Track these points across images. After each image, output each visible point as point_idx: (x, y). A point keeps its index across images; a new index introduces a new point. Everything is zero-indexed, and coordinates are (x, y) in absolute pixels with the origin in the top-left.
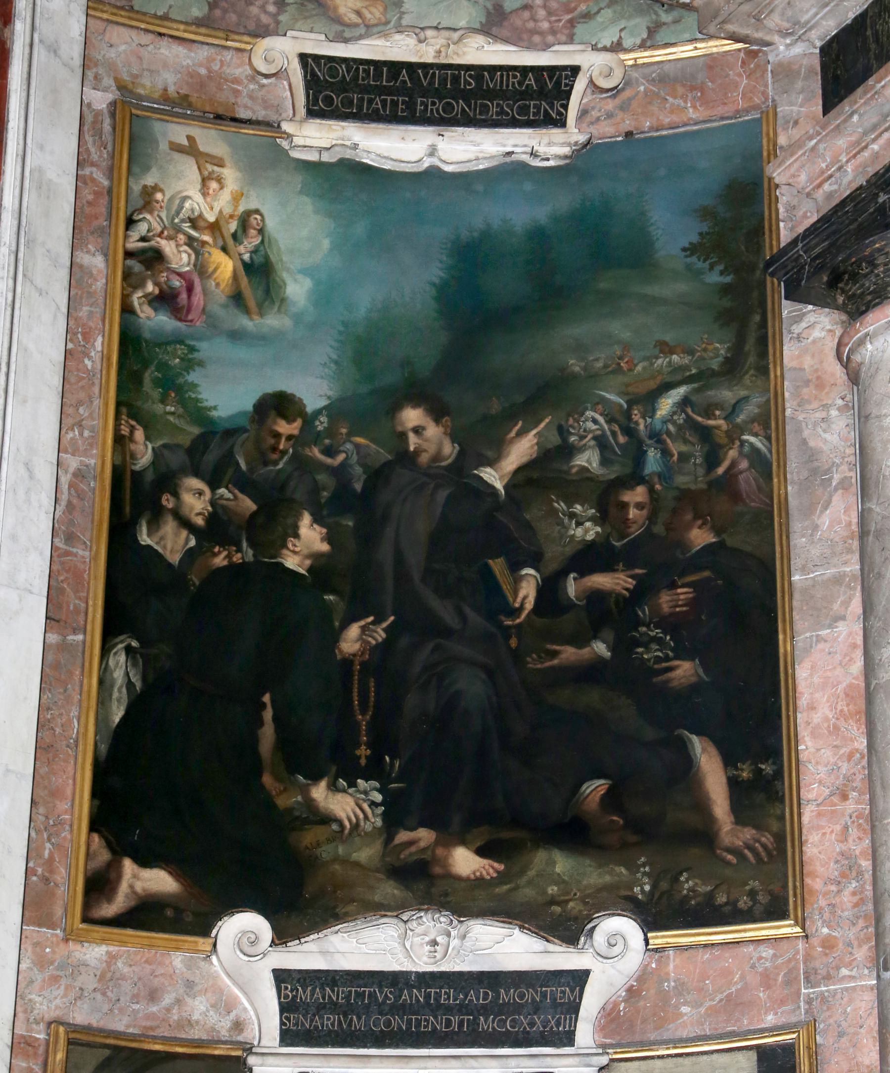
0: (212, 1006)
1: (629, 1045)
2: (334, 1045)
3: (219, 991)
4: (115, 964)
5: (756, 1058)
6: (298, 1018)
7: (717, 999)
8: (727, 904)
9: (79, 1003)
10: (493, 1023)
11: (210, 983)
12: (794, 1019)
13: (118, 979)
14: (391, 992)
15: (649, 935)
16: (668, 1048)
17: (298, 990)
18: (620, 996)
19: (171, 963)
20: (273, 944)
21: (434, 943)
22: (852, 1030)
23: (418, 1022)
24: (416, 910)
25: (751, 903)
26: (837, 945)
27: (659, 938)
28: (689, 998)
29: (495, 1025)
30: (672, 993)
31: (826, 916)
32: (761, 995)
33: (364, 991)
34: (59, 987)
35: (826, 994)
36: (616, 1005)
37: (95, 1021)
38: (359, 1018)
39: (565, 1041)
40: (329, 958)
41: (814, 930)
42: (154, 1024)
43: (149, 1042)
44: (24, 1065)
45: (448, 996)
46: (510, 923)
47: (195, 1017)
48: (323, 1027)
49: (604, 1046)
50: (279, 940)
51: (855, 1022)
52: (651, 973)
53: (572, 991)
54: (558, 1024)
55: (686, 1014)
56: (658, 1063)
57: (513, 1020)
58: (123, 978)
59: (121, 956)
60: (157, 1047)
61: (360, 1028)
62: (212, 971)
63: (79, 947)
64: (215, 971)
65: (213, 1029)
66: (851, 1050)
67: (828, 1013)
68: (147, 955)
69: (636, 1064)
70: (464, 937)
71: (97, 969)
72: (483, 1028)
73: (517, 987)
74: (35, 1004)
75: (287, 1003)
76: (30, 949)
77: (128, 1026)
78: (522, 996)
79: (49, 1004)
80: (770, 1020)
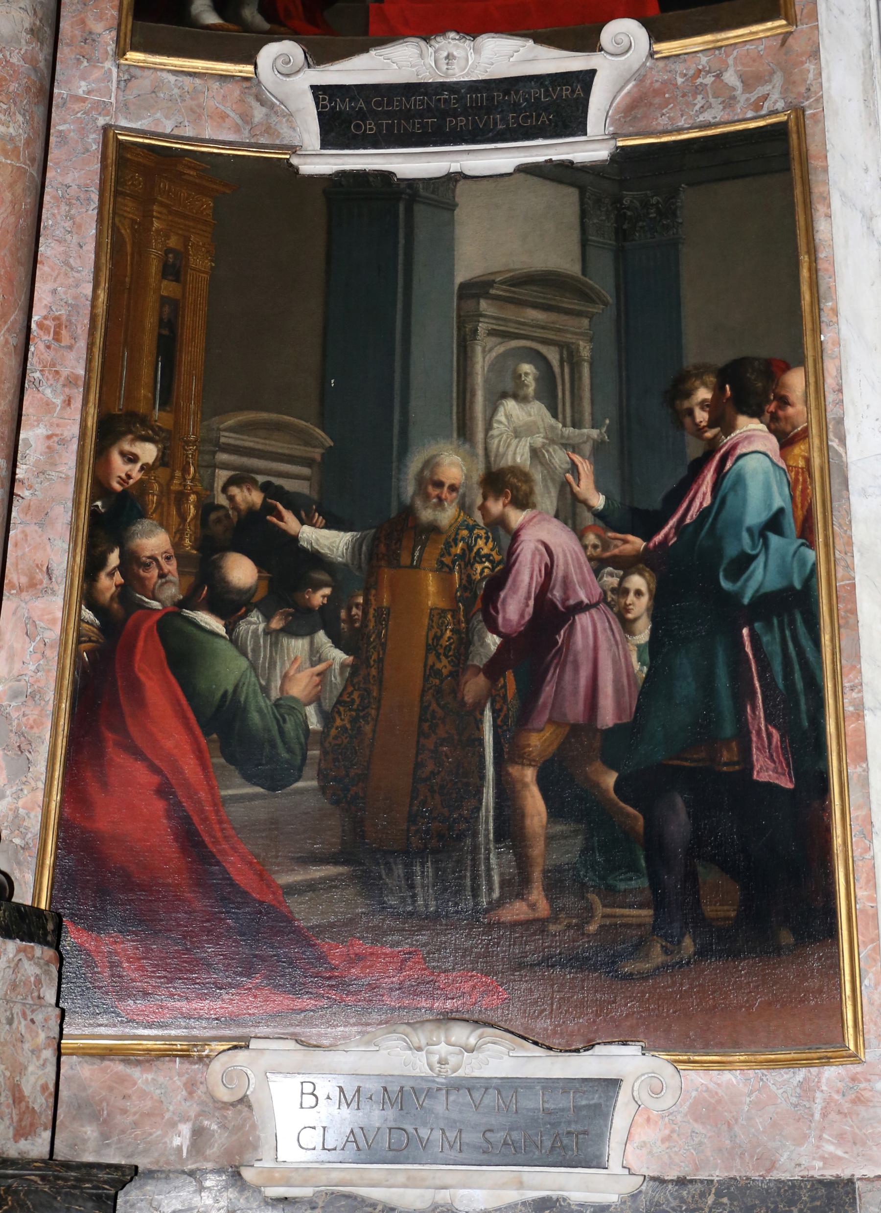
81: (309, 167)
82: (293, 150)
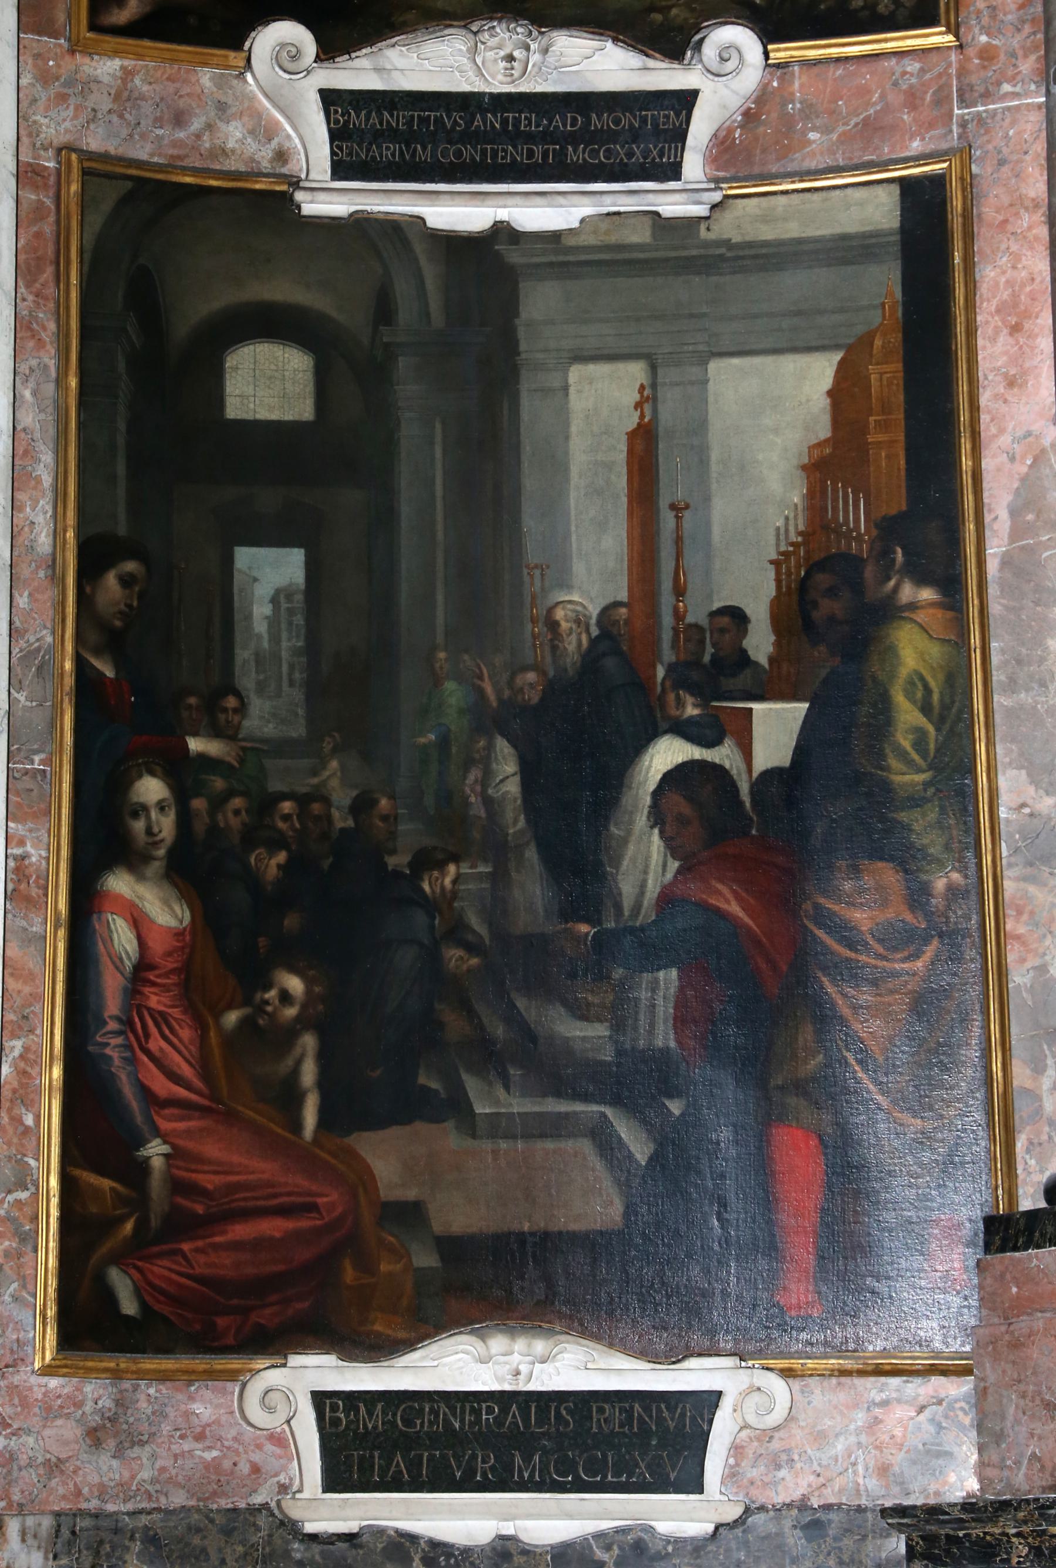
0: (249, 133)
1: (746, 179)
2: (395, 180)
3: (257, 115)
4: (132, 80)
5: (898, 192)
6: (352, 147)
7: (852, 123)
8: (863, 8)
9: (92, 126)
10: (584, 153)
11: (246, 105)
12: (944, 146)
13: (136, 99)
14: (460, 117)
15: (770, 47)
16: (793, 182)
17: (350, 114)
18: (735, 121)
19: (198, 81)
20: (318, 59)
21: (510, 58)
22: (1015, 157)
23: (495, 154)
24: (486, 19)
25: (892, 7)
26: (998, 56)
27: (781, 52)
28: (818, 122)
29: (586, 156)
30: (797, 117)
31: (985, 20)
32: (905, 117)
33: (429, 116)
34: (68, 107)
35: (984, 115)
36: (730, 131)
37: (112, 147)
38: (424, 148)
39: (669, 173)
40: (385, 76)
41: (970, 38)
42: (181, 152)
43: (178, 174)
44: (33, 197)
45: (529, 122)
46: (601, 34)
47: (231, 144)
48: (381, 157)
49: (717, 181)
50: (325, 54)
51: (1018, 147)
52: (772, 93)
53: (678, 115)
54: (661, 156)
55: (814, 141)
56: (782, 200)
57: (608, 150)
58: (142, 98)
59: (139, 72)
60: (188, 180)
61: (426, 159)
62: (247, 91)
63: (87, 60)
64: (251, 91)
65: (252, 160)
66: (1013, 181)
67: (985, 138)
68: (169, 71)
69: (755, 201)
70: (545, 51)
71: (111, 87)
72: (572, 160)
73: (611, 111)
74: (41, 126)
75: (338, 129)
76: (30, 61)
77: (152, 155)
78: (617, 122)
79: (57, 126)
80: (916, 146)
81: (313, 206)
82: (296, 183)
